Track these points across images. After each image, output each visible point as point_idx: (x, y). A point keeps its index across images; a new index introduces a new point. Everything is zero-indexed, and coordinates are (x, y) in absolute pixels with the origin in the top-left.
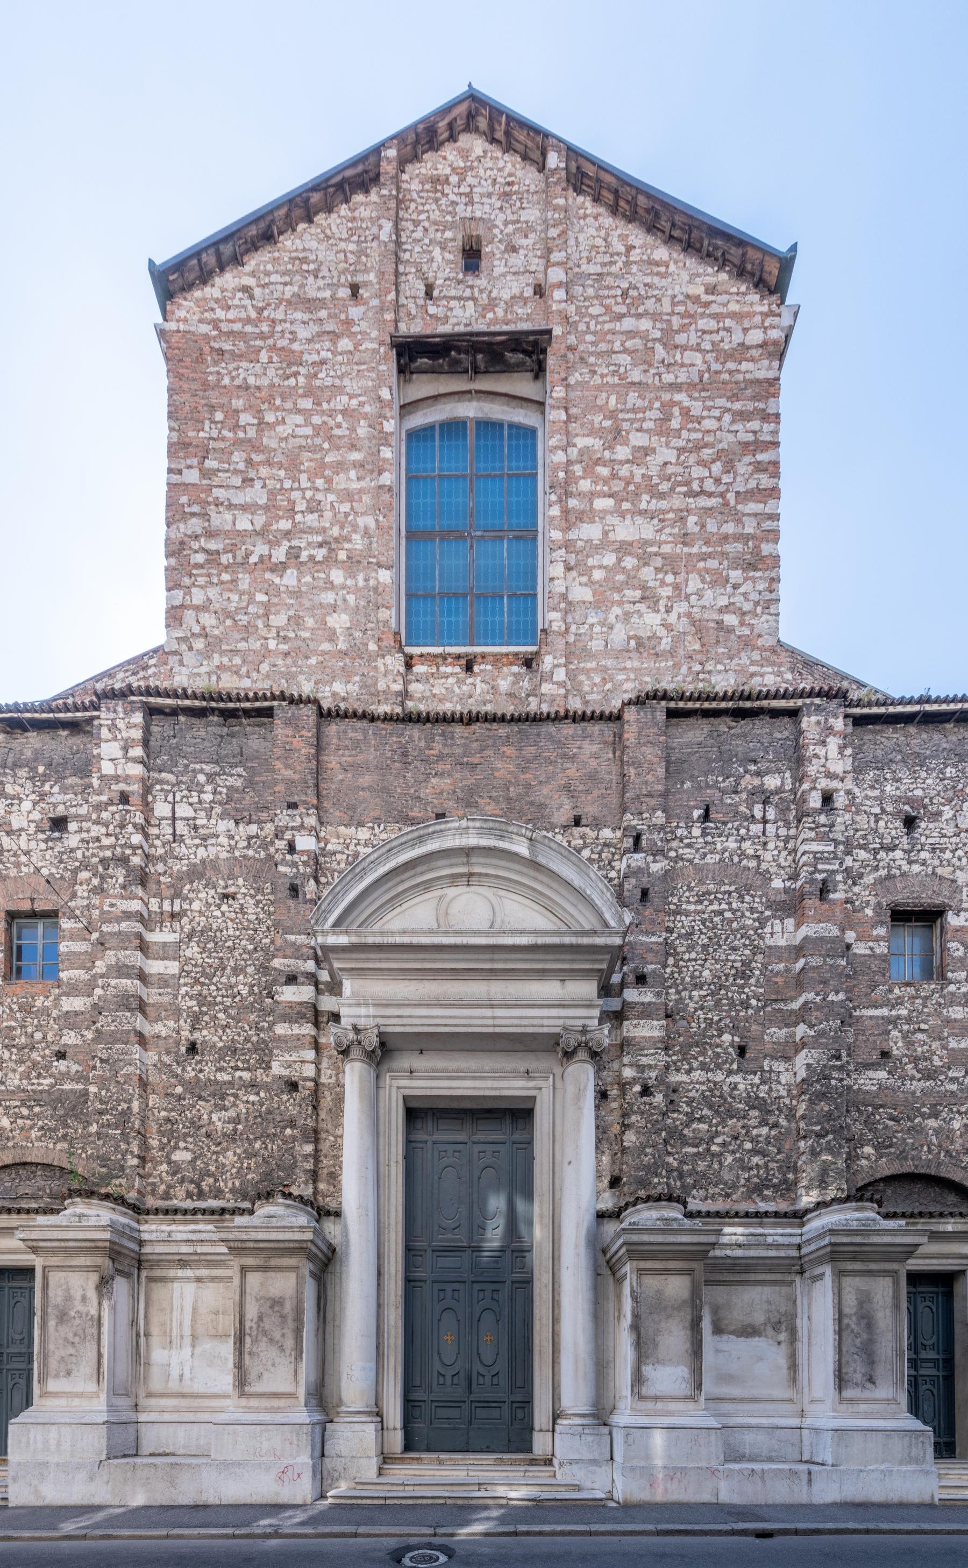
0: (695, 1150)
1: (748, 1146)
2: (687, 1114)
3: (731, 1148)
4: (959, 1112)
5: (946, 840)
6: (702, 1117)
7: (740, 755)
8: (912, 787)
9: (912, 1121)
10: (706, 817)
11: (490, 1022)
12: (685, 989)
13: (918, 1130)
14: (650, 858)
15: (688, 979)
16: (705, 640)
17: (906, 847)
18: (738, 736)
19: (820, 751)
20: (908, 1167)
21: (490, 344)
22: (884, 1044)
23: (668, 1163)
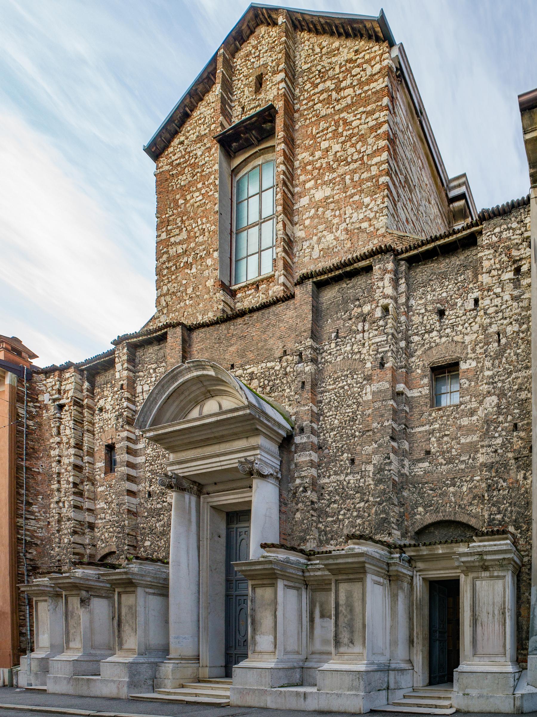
0: (332, 519)
1: (355, 514)
2: (328, 500)
4: (466, 481)
5: (459, 319)
6: (335, 501)
7: (352, 298)
10: (337, 337)
11: (219, 464)
12: (327, 432)
13: (444, 494)
14: (305, 365)
15: (328, 426)
16: (352, 241)
17: (438, 328)
18: (351, 288)
19: (381, 284)
20: (440, 517)
21: (253, 124)
22: (427, 447)
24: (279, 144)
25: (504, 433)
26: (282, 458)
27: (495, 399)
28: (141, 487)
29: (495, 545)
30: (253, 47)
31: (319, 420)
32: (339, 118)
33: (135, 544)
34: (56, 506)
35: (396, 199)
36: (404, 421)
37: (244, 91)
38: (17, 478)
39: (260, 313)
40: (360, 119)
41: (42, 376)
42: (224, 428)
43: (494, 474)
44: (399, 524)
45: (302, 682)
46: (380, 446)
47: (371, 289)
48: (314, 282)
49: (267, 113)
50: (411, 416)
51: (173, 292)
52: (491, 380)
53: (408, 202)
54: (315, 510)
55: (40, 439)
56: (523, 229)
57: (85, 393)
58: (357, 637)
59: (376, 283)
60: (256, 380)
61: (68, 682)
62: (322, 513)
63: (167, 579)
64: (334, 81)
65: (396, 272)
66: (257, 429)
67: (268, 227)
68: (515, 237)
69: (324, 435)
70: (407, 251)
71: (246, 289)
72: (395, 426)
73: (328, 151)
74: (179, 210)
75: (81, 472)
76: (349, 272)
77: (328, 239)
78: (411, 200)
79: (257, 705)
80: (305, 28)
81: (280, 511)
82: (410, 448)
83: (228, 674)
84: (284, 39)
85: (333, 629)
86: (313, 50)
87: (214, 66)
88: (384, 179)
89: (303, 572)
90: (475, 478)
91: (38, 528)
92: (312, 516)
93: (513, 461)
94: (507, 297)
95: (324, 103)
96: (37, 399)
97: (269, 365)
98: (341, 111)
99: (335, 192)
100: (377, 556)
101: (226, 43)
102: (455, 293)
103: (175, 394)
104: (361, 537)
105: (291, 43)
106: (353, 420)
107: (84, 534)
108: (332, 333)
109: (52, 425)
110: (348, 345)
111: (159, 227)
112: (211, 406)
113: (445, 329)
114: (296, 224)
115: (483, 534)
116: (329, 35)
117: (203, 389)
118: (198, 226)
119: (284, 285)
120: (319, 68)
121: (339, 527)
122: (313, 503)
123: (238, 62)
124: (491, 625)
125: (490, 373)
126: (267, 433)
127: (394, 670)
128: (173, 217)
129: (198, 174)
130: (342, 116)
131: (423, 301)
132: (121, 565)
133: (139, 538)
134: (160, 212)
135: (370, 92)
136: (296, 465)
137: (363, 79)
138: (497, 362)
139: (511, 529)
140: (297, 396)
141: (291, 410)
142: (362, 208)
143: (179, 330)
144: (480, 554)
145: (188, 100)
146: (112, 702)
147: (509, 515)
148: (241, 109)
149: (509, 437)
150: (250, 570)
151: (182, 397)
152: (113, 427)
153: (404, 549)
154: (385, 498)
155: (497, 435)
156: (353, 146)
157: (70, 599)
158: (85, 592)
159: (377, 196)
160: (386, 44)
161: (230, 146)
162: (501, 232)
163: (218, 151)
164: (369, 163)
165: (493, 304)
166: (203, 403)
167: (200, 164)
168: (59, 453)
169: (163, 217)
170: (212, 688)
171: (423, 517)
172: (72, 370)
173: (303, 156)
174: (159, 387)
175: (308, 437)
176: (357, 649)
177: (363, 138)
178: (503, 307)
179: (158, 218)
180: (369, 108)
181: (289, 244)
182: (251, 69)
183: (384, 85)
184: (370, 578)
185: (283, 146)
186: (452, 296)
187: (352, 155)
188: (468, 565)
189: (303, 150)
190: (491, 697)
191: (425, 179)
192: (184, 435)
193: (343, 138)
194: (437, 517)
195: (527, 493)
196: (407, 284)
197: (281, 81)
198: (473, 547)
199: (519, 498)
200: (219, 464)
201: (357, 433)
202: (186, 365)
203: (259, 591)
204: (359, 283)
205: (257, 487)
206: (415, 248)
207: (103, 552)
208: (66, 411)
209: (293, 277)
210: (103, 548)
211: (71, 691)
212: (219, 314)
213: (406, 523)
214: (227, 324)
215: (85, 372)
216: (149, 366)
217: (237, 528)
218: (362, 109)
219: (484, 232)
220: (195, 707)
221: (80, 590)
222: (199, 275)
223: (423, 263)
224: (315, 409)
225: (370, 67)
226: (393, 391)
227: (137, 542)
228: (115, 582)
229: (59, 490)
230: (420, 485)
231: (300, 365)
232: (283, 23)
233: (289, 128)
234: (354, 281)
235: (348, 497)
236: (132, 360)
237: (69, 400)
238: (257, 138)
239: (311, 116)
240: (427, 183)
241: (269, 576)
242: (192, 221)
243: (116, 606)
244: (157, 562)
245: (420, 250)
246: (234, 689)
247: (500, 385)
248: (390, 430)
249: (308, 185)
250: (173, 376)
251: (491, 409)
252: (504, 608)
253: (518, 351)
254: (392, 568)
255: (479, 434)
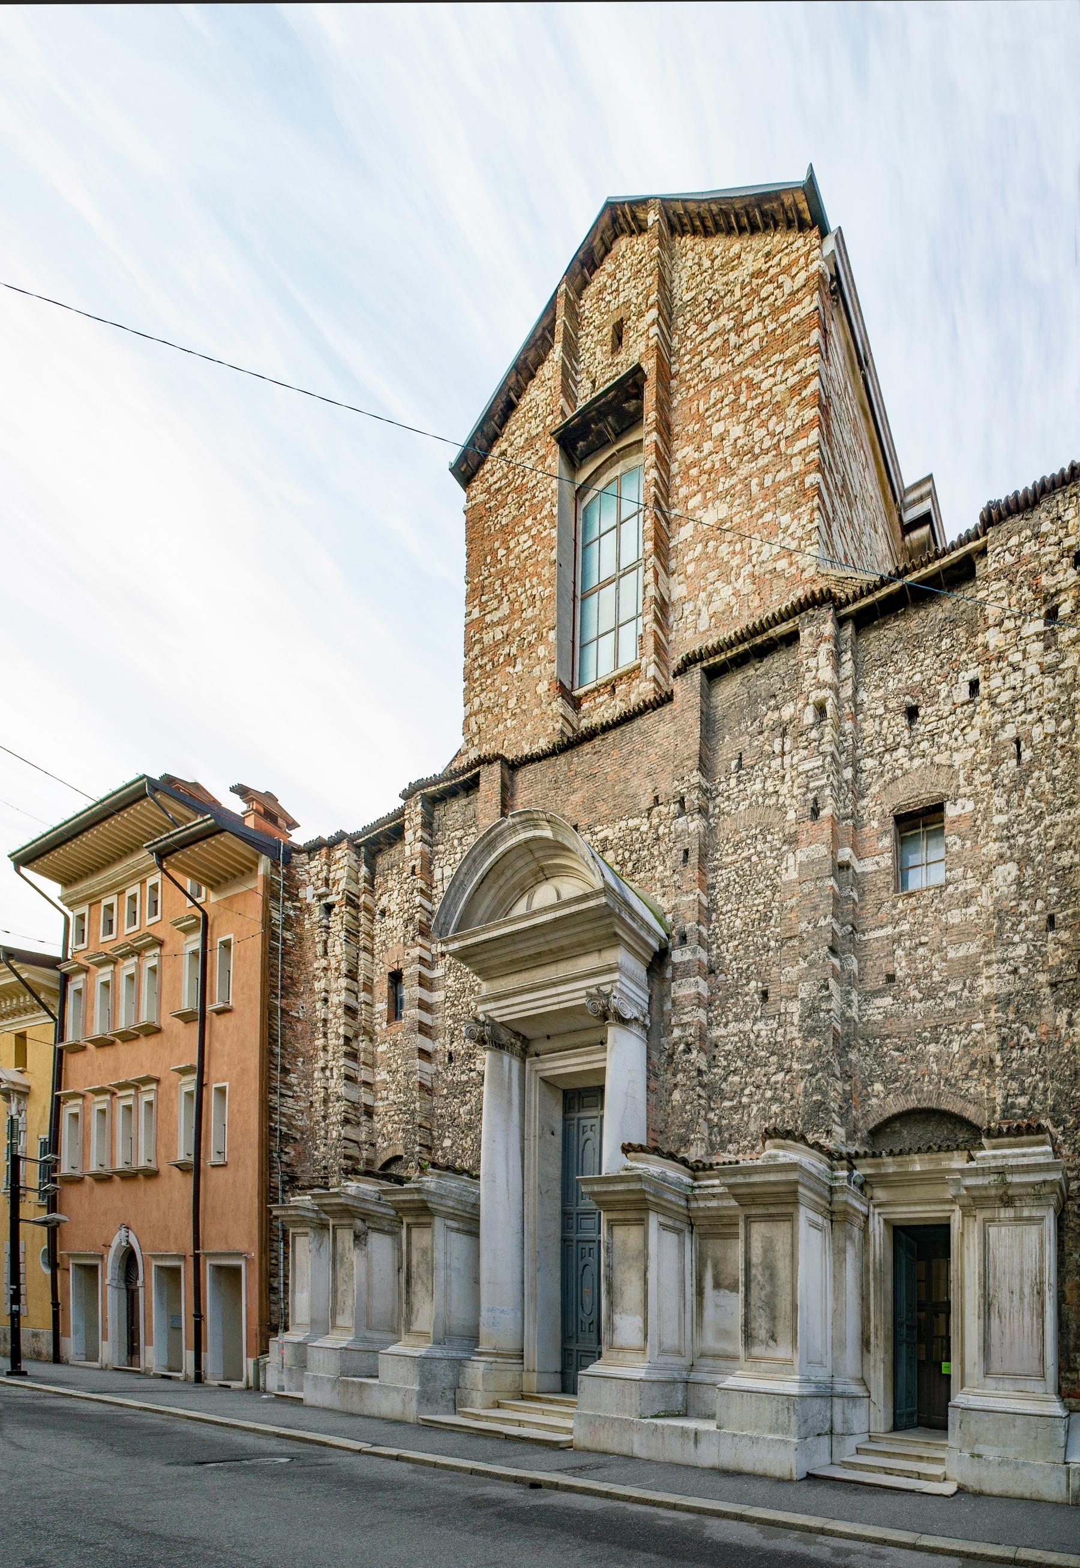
1: (769, 1094)
2: (724, 1068)
3: (756, 1098)
4: (958, 1033)
5: (943, 721)
8: (911, 673)
9: (915, 1050)
10: (740, 766)
11: (555, 1000)
12: (724, 942)
15: (725, 932)
17: (908, 742)
19: (812, 663)
20: (911, 1102)
24: (648, 433)
25: (1030, 935)
26: (652, 990)
27: (1012, 868)
28: (438, 1045)
29: (1024, 1155)
30: (609, 276)
31: (710, 921)
32: (742, 379)
33: (429, 1143)
34: (321, 1075)
35: (831, 516)
36: (850, 918)
37: (595, 353)
38: (271, 1027)
39: (618, 731)
40: (773, 376)
41: (304, 857)
42: (565, 933)
43: (1012, 1017)
44: (844, 1115)
45: (686, 1409)
46: (812, 965)
47: (797, 676)
48: (703, 669)
49: (631, 381)
50: (862, 909)
51: (488, 707)
52: (1005, 832)
53: (847, 524)
54: (703, 1086)
55: (302, 963)
56: (1062, 533)
57: (362, 885)
58: (783, 1328)
59: (805, 662)
60: (611, 852)
61: (334, 1387)
62: (714, 1092)
63: (476, 1206)
64: (732, 315)
65: (837, 640)
66: (616, 934)
67: (629, 582)
68: (1048, 549)
69: (718, 947)
70: (855, 599)
71: (596, 694)
72: (836, 926)
73: (723, 439)
74: (499, 566)
75: (354, 1019)
76: (761, 645)
77: (723, 595)
78: (851, 523)
79: (617, 1450)
80: (688, 228)
81: (648, 1087)
82: (861, 969)
83: (567, 1385)
84: (657, 249)
85: (741, 1311)
86: (700, 265)
87: (551, 314)
88: (814, 478)
89: (687, 1200)
90: (974, 1027)
91: (298, 1111)
92: (699, 1096)
93: (1047, 990)
94: (1032, 669)
95: (716, 355)
96: (297, 895)
97: (632, 823)
98: (743, 365)
99: (734, 510)
100: (813, 1170)
101: (569, 273)
102: (936, 674)
103: (492, 875)
104: (788, 1134)
105: (665, 257)
106: (766, 918)
107: (358, 1124)
108: (732, 759)
109: (317, 940)
110: (758, 780)
111: (469, 599)
112: (544, 895)
113: (919, 743)
114: (673, 574)
115: (1000, 1134)
116: (724, 235)
117: (533, 866)
118: (525, 591)
119: (655, 680)
120: (709, 294)
121: (742, 1119)
122: (700, 1072)
123: (587, 304)
124: (1016, 1315)
125: (1001, 819)
126: (633, 944)
127: (841, 1396)
128: (490, 580)
129: (527, 504)
130: (745, 373)
131: (882, 691)
132: (409, 1178)
133: (435, 1134)
134: (471, 572)
135: (789, 325)
136: (673, 1002)
137: (778, 303)
138: (1015, 796)
139: (1046, 1122)
140: (676, 877)
141: (665, 904)
142: (777, 535)
143: (497, 767)
144: (1001, 1172)
145: (513, 380)
146: (394, 1428)
147: (1041, 1097)
148: (590, 385)
149: (1039, 943)
150: (606, 1192)
151: (501, 882)
152: (399, 942)
153: (855, 1162)
154: (820, 1065)
155: (1016, 939)
156: (763, 424)
157: (339, 1232)
158: (360, 1221)
159: (800, 510)
160: (815, 232)
161: (575, 449)
162: (1021, 544)
163: (558, 457)
164: (789, 452)
165: (1007, 686)
166: (532, 890)
167: (530, 485)
168: (326, 991)
169: (476, 581)
170: (544, 1412)
171: (884, 1102)
172: (344, 845)
173: (684, 452)
174: (469, 861)
175: (694, 951)
176: (783, 1351)
177: (778, 409)
178: (1026, 689)
179: (468, 583)
180: (788, 354)
181: (663, 607)
182: (606, 313)
183: (812, 308)
184: (804, 1214)
185: (654, 436)
186: (930, 679)
187: (762, 441)
188: (976, 1193)
189: (684, 443)
190: (1024, 1464)
191: (870, 488)
192: (504, 947)
193: (748, 413)
194: (907, 1101)
195: (1074, 1052)
196: (854, 662)
197: (653, 324)
198: (983, 1158)
199: (1060, 1063)
200: (555, 1000)
201: (772, 943)
202: (510, 821)
203: (619, 1232)
204: (776, 665)
205: (615, 1041)
206: (870, 592)
207: (385, 1157)
208: (336, 915)
209: (667, 668)
210: (384, 1149)
211: (337, 1405)
212: (556, 739)
213: (854, 1113)
214: (568, 754)
215: (363, 849)
216: (453, 834)
217: (579, 1119)
218: (776, 358)
219: (989, 549)
220: (519, 1447)
221: (354, 1217)
222: (526, 676)
223: (881, 621)
224: (705, 901)
225: (789, 279)
226: (834, 860)
227: (433, 1139)
228: (402, 1205)
229: (325, 1049)
230: (878, 1041)
231: (680, 820)
232: (655, 222)
233: (664, 405)
234: (767, 662)
235: (758, 1063)
236: (428, 825)
237: (340, 897)
238: (614, 430)
239: (696, 381)
240: (873, 494)
241: (635, 1204)
242: (517, 585)
243: (404, 1247)
244: (461, 1174)
245: (878, 595)
246: (580, 1416)
247: (1021, 840)
248: (830, 935)
249: (692, 503)
250: (489, 842)
251: (1005, 889)
252: (1042, 1283)
253: (1055, 772)
254: (839, 1197)
255: (980, 940)
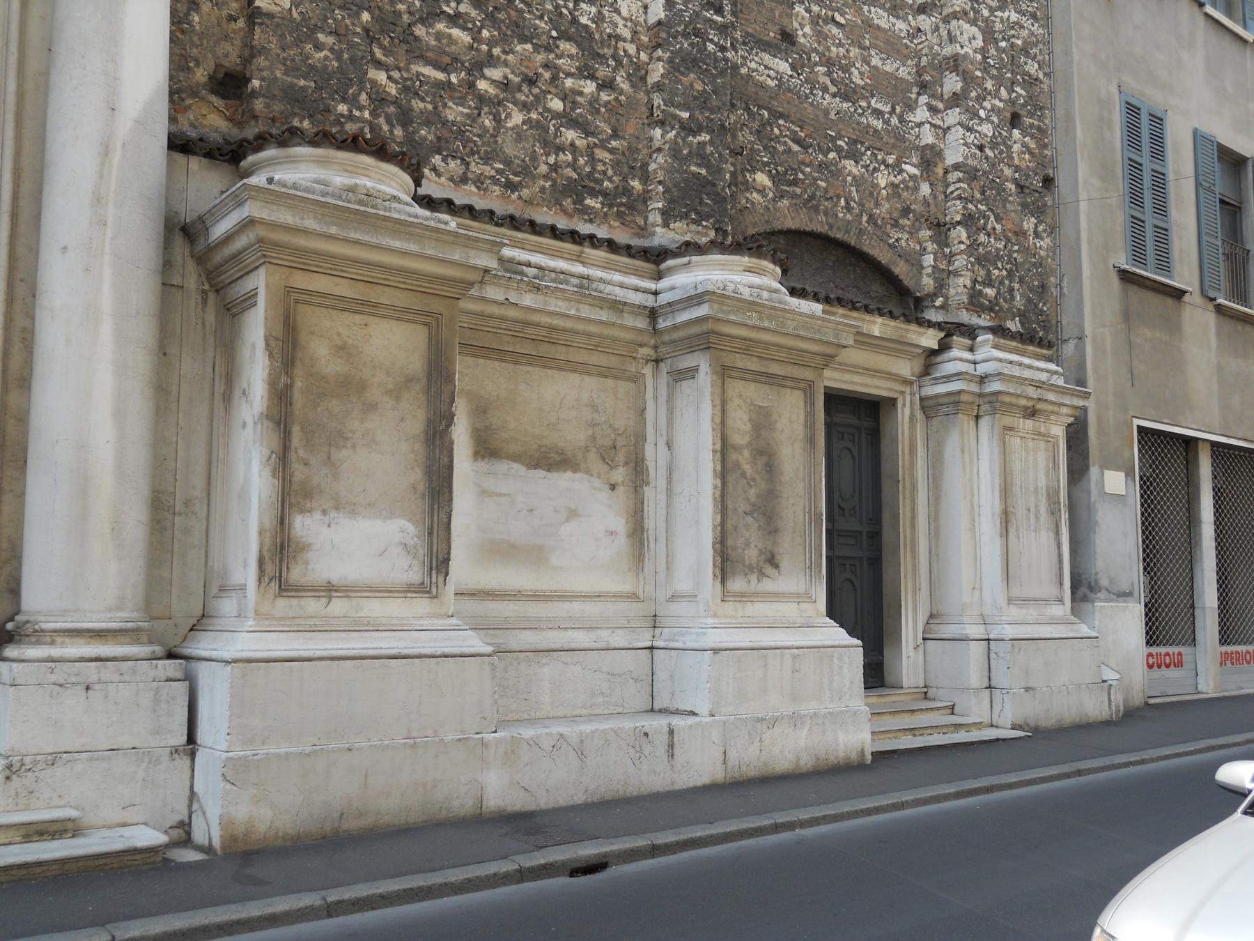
9: (826, 155)
20: (818, 225)
23: (374, 83)
